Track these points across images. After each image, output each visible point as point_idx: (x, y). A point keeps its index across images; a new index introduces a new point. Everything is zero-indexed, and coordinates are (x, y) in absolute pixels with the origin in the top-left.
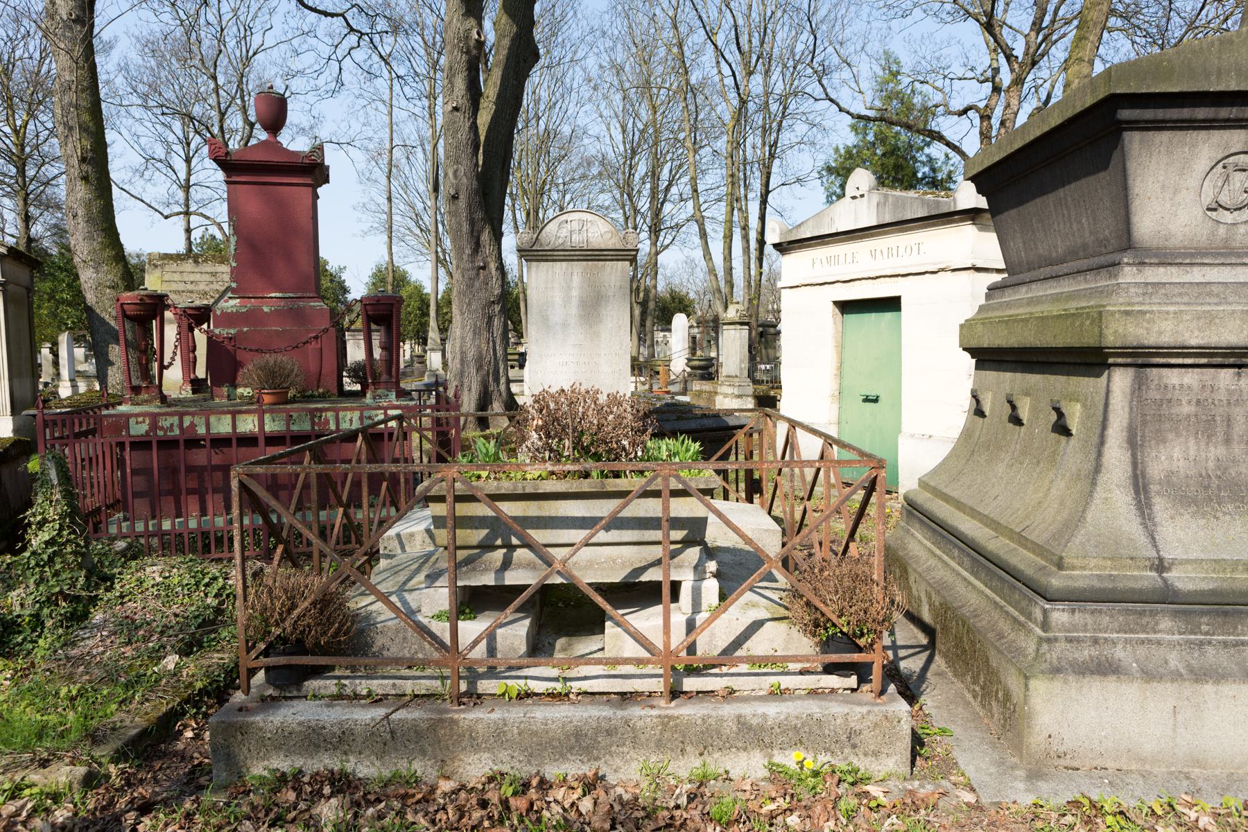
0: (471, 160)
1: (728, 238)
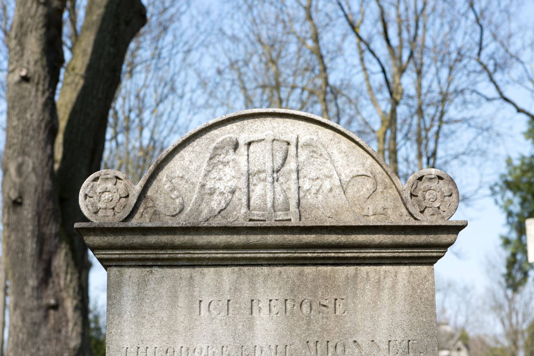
0: (44, 150)
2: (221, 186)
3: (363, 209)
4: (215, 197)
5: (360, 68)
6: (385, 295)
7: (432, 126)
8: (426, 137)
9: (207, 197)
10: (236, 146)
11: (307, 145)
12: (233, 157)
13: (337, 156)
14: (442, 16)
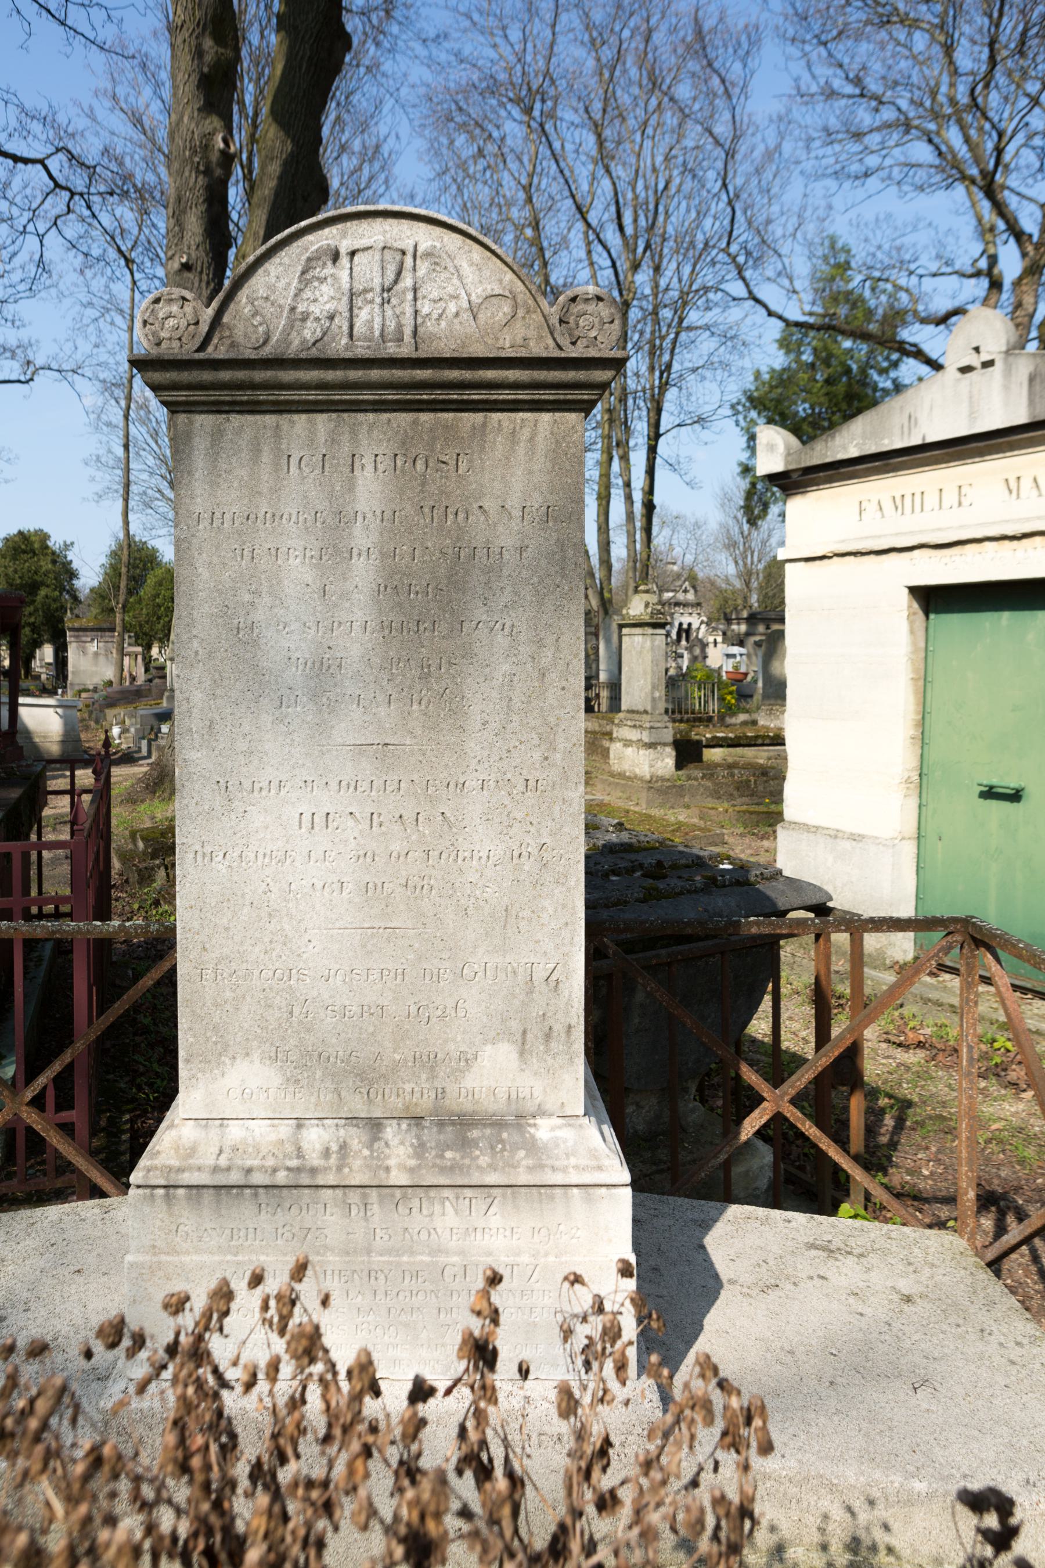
1: (604, 499)
2: (316, 310)
3: (497, 339)
4: (309, 324)
5: (586, 263)
6: (521, 449)
7: (668, 334)
8: (661, 347)
9: (298, 323)
10: (336, 257)
11: (428, 254)
12: (332, 271)
13: (466, 269)
14: (689, 197)
